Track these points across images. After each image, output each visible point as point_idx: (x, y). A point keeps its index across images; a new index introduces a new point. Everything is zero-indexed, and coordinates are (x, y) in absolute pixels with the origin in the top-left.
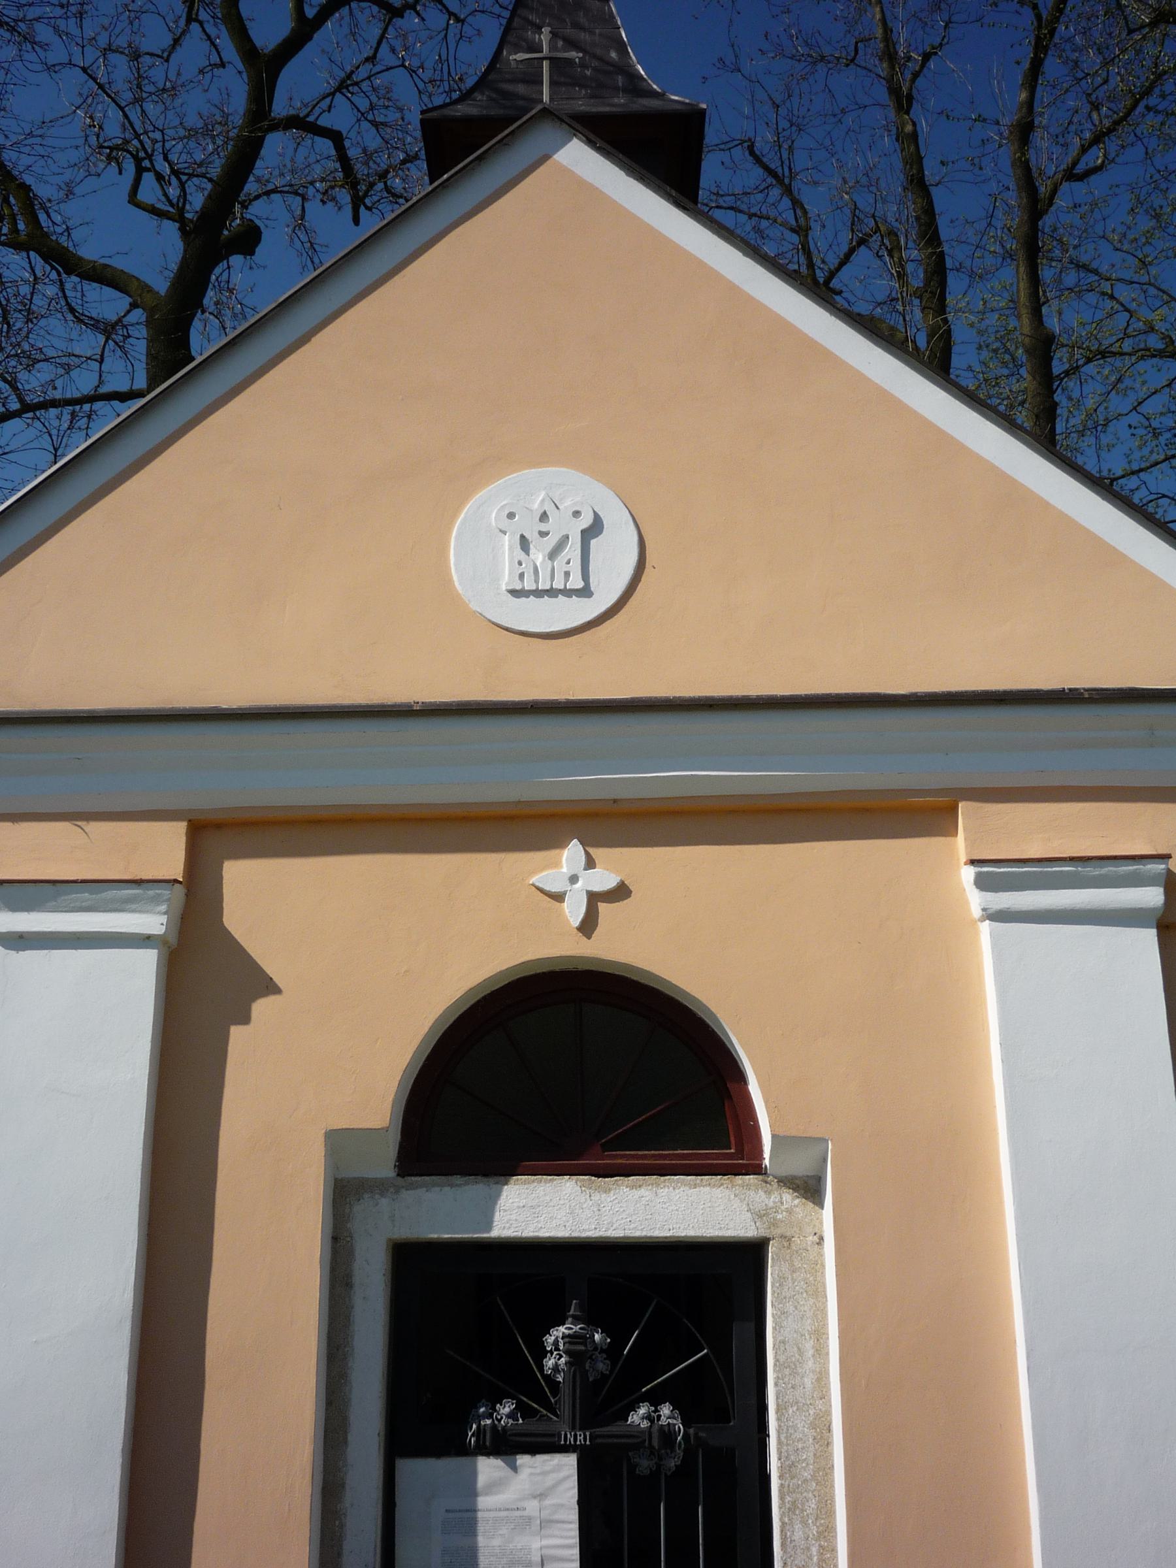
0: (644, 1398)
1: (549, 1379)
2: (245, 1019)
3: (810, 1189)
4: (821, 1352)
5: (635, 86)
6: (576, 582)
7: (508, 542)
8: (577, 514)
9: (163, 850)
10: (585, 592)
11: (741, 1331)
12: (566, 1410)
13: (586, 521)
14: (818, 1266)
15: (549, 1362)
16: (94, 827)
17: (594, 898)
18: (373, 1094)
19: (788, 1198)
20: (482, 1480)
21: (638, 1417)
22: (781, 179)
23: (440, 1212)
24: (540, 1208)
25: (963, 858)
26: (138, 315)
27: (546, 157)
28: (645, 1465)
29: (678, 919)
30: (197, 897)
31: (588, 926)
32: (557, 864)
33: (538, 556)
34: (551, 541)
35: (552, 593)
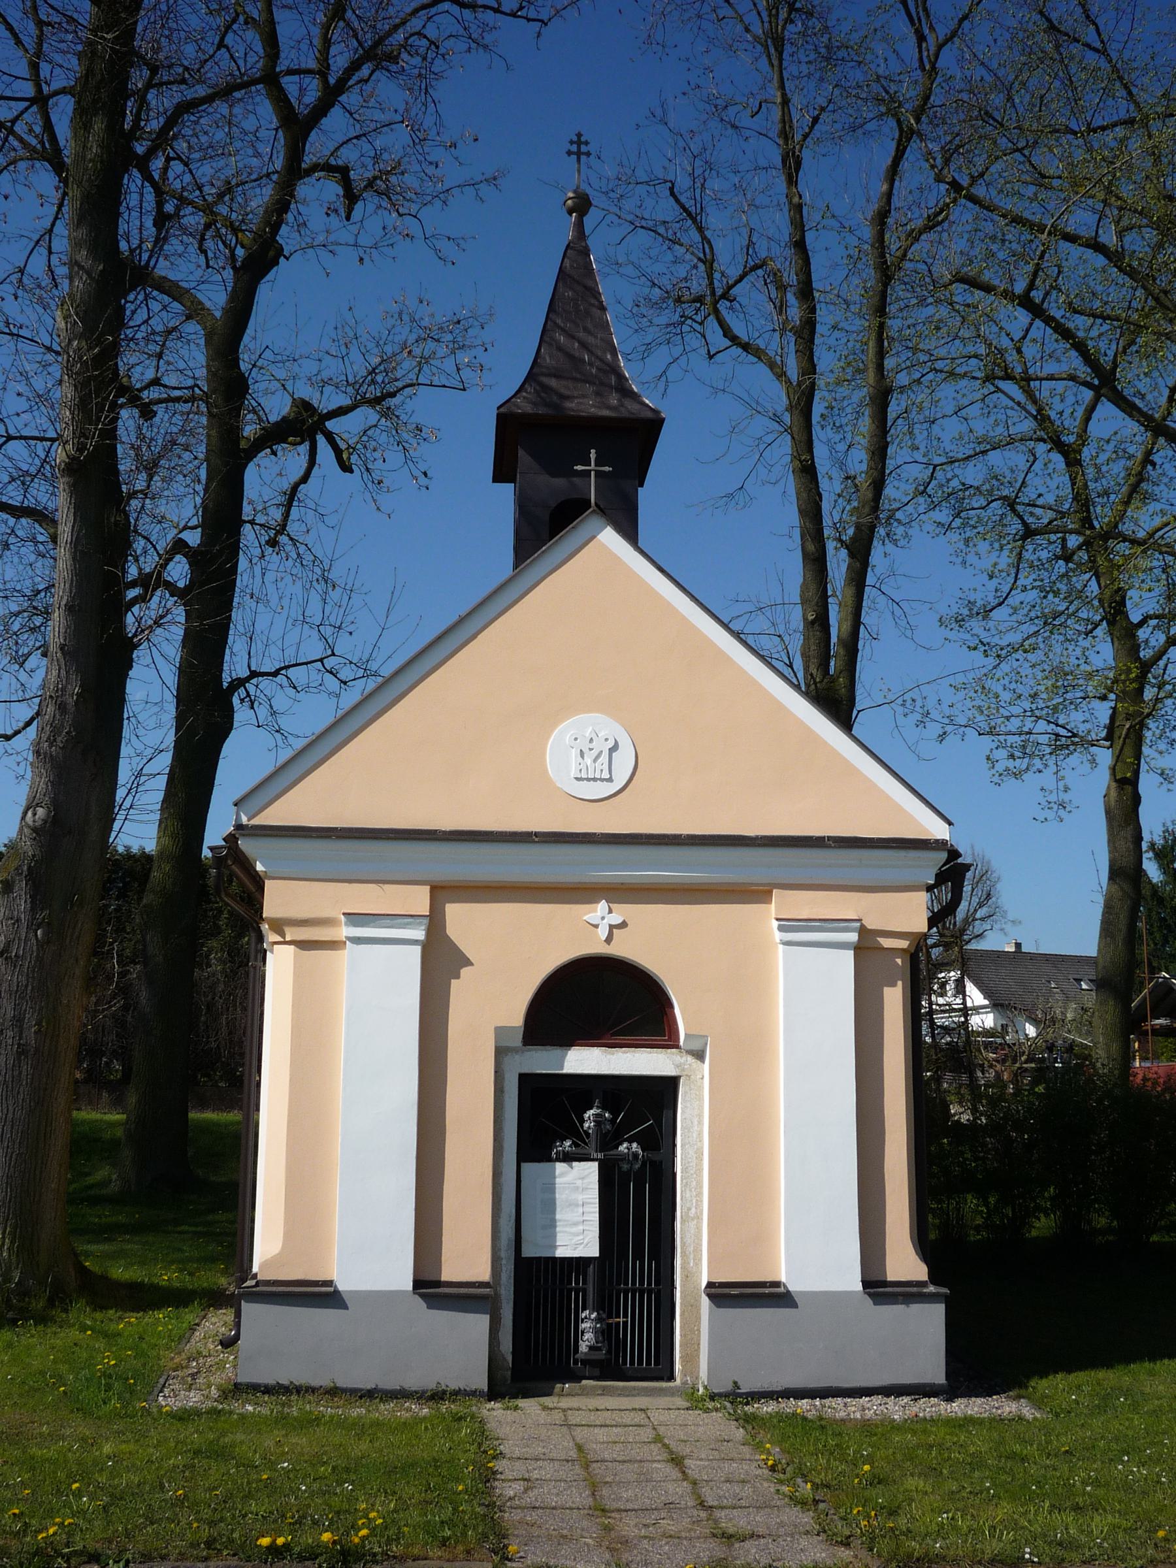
0: (625, 1140)
1: (586, 1133)
2: (458, 977)
3: (699, 1055)
4: (700, 1123)
5: (626, 392)
6: (606, 775)
7: (574, 753)
8: (606, 740)
9: (418, 900)
10: (610, 780)
11: (666, 1114)
12: (594, 1146)
13: (611, 744)
14: (701, 1088)
15: (586, 1125)
16: (386, 887)
17: (611, 927)
18: (513, 1011)
19: (690, 1059)
20: (557, 1172)
21: (623, 1148)
22: (694, 218)
23: (541, 1061)
24: (584, 1060)
25: (774, 916)
26: (192, 327)
27: (594, 537)
28: (625, 1167)
29: (646, 936)
30: (435, 922)
31: (609, 940)
32: (595, 911)
33: (588, 760)
34: (594, 753)
35: (595, 779)
